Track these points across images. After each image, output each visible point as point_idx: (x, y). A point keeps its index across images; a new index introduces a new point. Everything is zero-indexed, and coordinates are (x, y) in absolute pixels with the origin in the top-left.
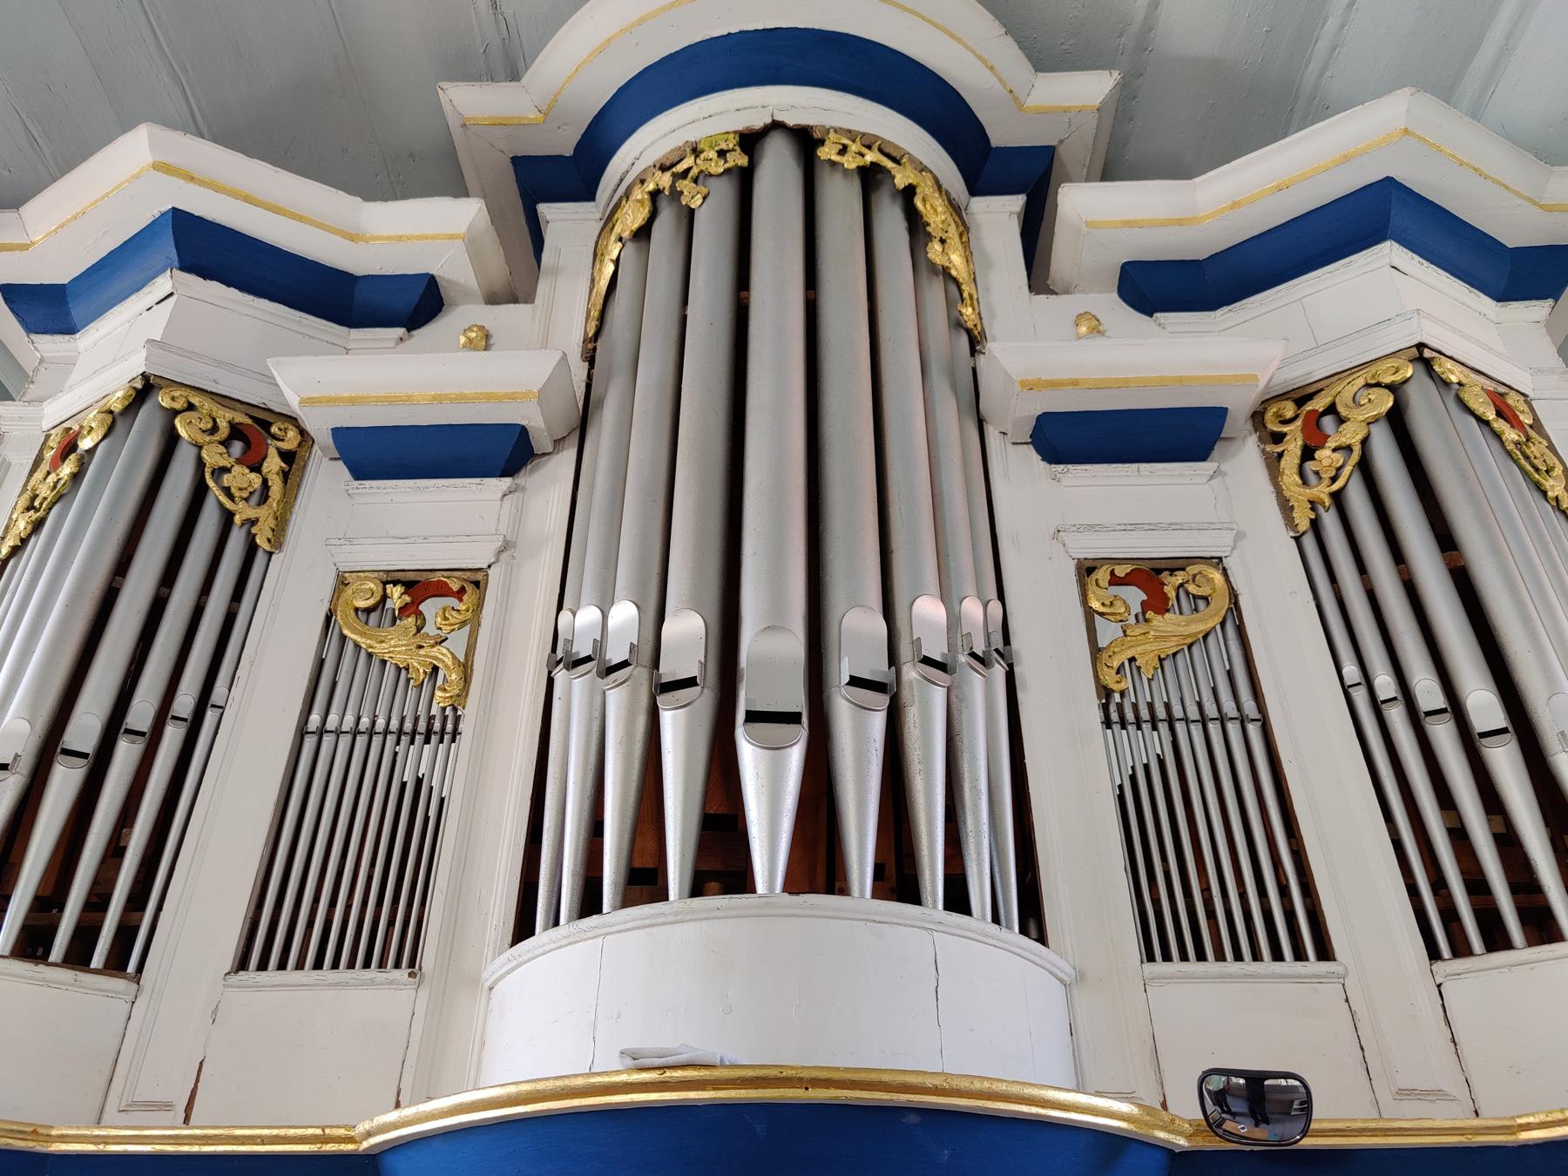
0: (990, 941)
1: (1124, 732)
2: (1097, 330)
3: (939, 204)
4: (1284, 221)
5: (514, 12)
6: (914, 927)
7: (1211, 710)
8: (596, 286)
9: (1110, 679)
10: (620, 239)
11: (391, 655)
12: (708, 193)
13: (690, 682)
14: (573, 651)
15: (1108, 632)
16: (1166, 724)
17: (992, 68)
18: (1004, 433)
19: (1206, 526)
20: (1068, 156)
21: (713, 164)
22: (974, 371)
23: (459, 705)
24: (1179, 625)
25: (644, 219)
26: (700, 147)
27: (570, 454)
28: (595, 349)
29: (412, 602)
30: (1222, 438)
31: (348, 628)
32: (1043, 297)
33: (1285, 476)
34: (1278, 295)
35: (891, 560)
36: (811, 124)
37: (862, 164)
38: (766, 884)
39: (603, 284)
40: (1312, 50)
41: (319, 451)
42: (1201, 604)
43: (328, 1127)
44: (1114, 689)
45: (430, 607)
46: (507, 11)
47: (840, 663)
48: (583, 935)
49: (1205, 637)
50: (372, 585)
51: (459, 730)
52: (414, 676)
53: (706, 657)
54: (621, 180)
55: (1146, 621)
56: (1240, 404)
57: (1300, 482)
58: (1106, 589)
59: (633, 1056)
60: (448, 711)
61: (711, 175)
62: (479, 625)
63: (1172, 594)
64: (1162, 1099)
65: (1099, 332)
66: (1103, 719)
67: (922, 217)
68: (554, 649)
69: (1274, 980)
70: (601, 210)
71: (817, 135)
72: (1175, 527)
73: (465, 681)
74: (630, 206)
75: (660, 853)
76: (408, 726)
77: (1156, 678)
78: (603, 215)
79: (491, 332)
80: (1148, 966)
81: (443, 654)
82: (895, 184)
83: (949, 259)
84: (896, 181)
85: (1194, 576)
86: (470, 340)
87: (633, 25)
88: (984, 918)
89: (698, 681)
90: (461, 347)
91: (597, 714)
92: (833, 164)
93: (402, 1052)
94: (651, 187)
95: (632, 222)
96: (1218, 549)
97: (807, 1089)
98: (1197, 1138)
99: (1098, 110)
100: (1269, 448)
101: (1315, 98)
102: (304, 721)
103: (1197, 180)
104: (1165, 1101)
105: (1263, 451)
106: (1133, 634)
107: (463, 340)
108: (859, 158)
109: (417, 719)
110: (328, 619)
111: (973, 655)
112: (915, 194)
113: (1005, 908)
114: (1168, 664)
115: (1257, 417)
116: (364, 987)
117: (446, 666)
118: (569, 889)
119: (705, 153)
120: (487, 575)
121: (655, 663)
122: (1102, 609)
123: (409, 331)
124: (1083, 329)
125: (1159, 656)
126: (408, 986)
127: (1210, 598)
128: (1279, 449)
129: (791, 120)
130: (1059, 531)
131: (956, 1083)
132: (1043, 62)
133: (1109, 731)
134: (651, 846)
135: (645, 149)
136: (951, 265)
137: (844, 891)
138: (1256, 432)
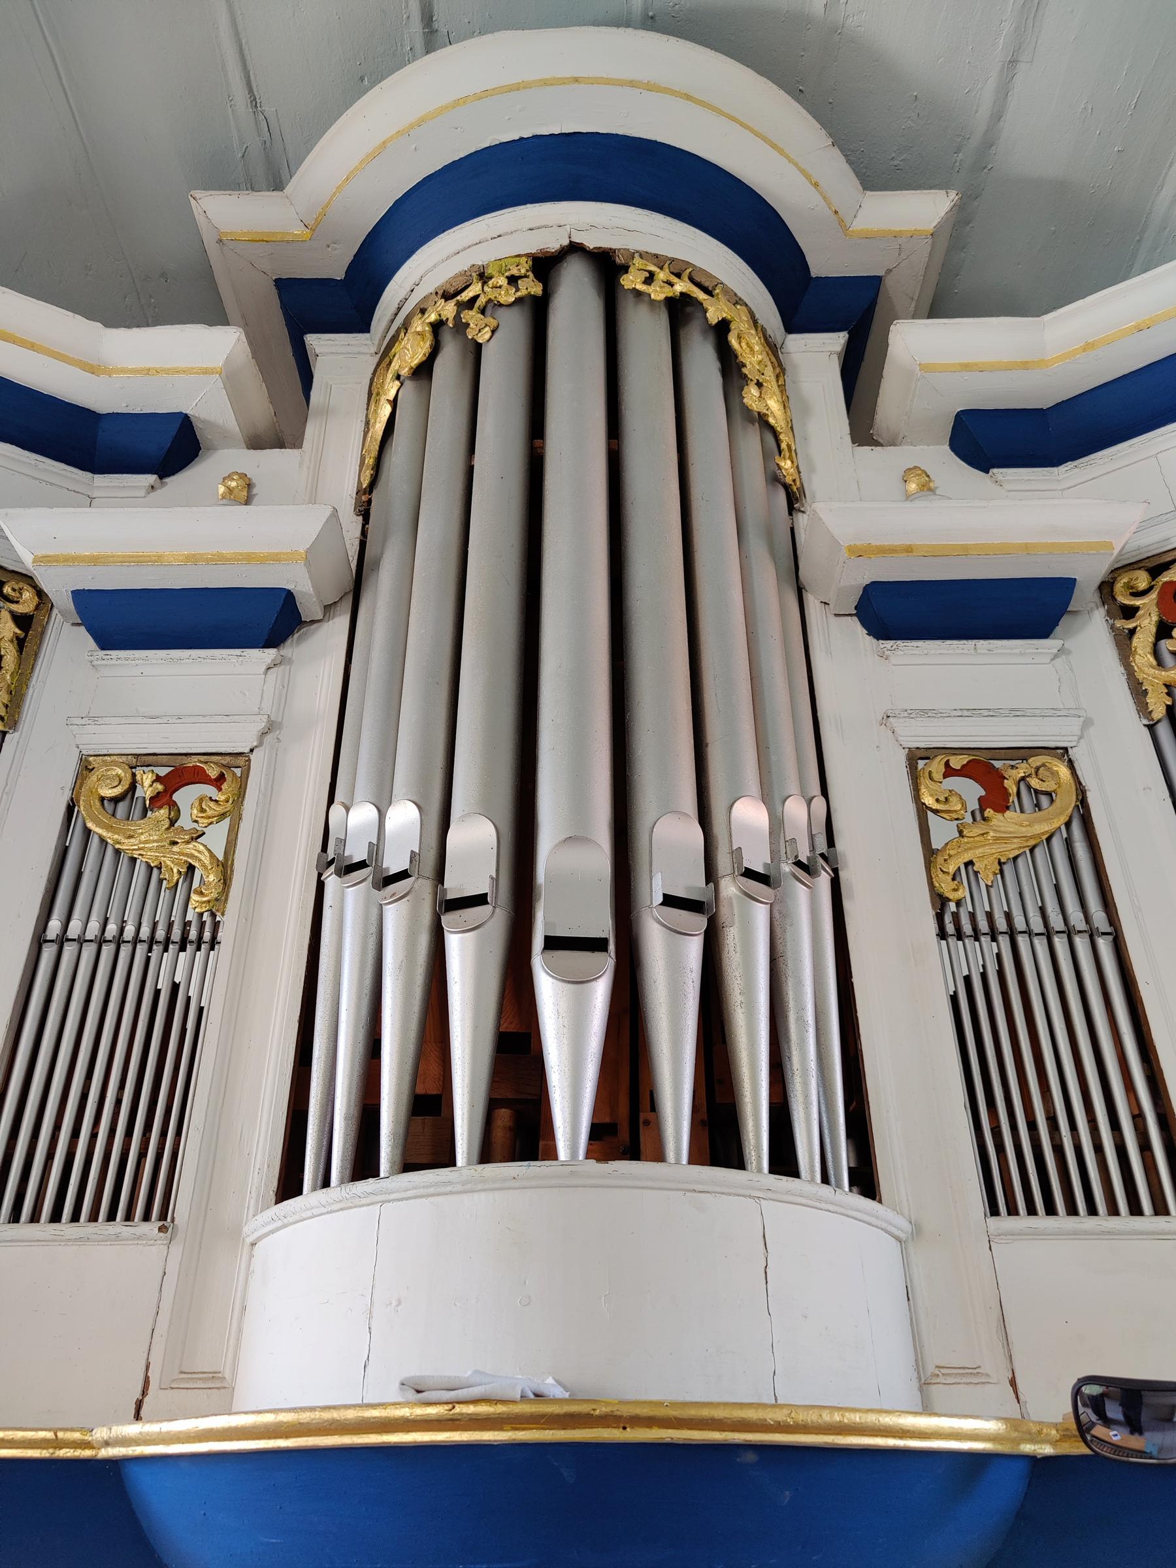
0: (823, 1205)
1: (960, 943)
2: (927, 488)
3: (756, 342)
4: (1141, 366)
6: (738, 1195)
7: (1056, 922)
8: (371, 430)
9: (945, 886)
10: (398, 377)
11: (142, 852)
12: (498, 327)
13: (481, 900)
14: (345, 855)
15: (942, 832)
16: (1007, 938)
17: (816, 185)
18: (825, 603)
19: (1051, 712)
20: (898, 289)
21: (503, 293)
22: (792, 530)
23: (217, 910)
25: (425, 355)
26: (489, 271)
27: (342, 622)
28: (369, 502)
29: (165, 791)
30: (1069, 611)
31: (92, 820)
32: (867, 448)
33: (1137, 656)
34: (1131, 450)
35: (706, 755)
36: (613, 247)
37: (670, 295)
38: (568, 1143)
39: (379, 427)
40: (1166, 174)
41: (59, 615)
42: (1044, 800)
43: (61, 1430)
44: (951, 897)
45: (186, 796)
46: (269, 109)
47: (651, 879)
48: (357, 1201)
49: (1049, 840)
50: (120, 771)
51: (218, 939)
52: (167, 877)
53: (497, 871)
54: (399, 309)
55: (984, 819)
57: (1154, 663)
58: (941, 782)
59: (416, 1387)
60: (206, 917)
61: (501, 305)
62: (240, 819)
63: (1013, 789)
64: (1010, 1376)
65: (930, 490)
66: (938, 931)
67: (736, 357)
68: (324, 848)
69: (1135, 1237)
70: (376, 342)
71: (620, 260)
72: (1017, 713)
73: (225, 883)
74: (408, 340)
75: (444, 1078)
76: (160, 934)
77: (995, 884)
78: (380, 345)
79: (254, 481)
80: (992, 1221)
81: (199, 852)
82: (706, 319)
83: (767, 405)
84: (707, 314)
85: (1037, 769)
86: (230, 490)
87: (411, 127)
88: (813, 1180)
89: (489, 899)
90: (220, 497)
91: (373, 929)
92: (638, 294)
93: (151, 1321)
94: (433, 317)
95: (412, 358)
96: (1065, 738)
97: (624, 1428)
98: (1063, 1444)
99: (932, 235)
100: (1119, 623)
101: (1165, 228)
102: (42, 927)
103: (1047, 318)
104: (1014, 1377)
105: (1112, 627)
106: (971, 834)
107: (222, 489)
108: (667, 288)
109: (170, 925)
110: (70, 809)
111: (799, 864)
112: (729, 330)
113: (832, 1153)
114: (1008, 869)
115: (1106, 589)
116: (109, 1243)
117: (204, 865)
118: (342, 1135)
119: (493, 280)
120: (249, 760)
121: (440, 875)
122: (936, 806)
123: (161, 478)
124: (912, 487)
125: (999, 860)
126: (158, 1242)
127: (1054, 795)
128: (1131, 625)
129: (591, 242)
130: (888, 717)
131: (802, 1417)
133: (944, 942)
134: (435, 1069)
135: (426, 274)
136: (769, 413)
137: (659, 1156)
138: (1104, 605)
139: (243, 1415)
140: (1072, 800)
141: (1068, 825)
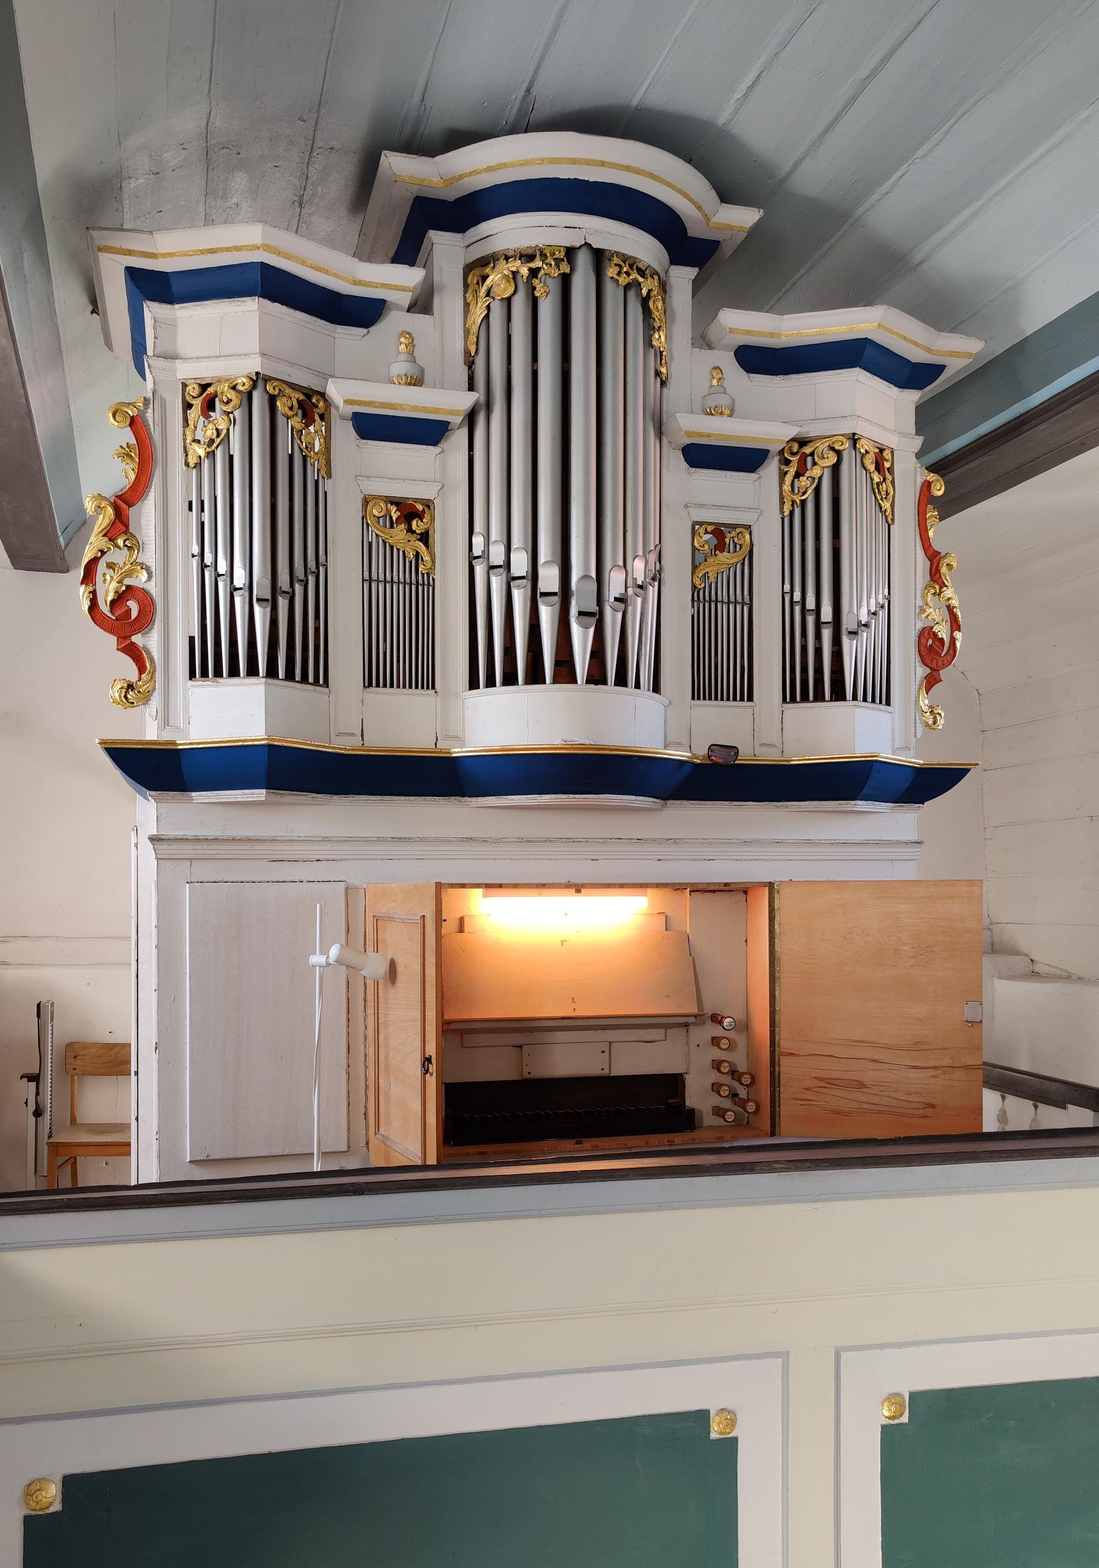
5: (432, 106)
9: (697, 582)
24: (728, 559)
27: (465, 431)
56: (775, 448)
82: (641, 293)
100: (783, 467)
105: (780, 468)
132: (726, 196)
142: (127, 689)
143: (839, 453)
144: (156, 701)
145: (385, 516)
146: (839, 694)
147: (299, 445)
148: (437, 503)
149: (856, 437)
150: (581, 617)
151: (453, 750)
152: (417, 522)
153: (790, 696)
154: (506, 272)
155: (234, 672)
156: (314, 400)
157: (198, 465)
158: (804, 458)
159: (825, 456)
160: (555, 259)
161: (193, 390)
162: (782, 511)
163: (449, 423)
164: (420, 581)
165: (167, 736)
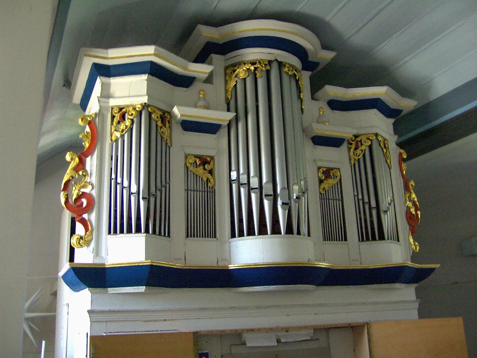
9: (321, 191)
27: (226, 130)
88: (306, 236)
100: (349, 146)
105: (348, 146)
132: (325, 47)
139: (125, 263)
140: (339, 178)
141: (337, 183)
142: (80, 239)
143: (371, 140)
144: (93, 244)
145: (194, 163)
146: (382, 237)
147: (161, 134)
148: (216, 158)
149: (377, 135)
150: (283, 205)
151: (229, 266)
152: (208, 165)
153: (362, 239)
154: (245, 69)
155: (129, 231)
156: (166, 115)
157: (117, 141)
158: (357, 142)
159: (366, 141)
160: (264, 64)
161: (116, 110)
162: (350, 163)
163: (222, 125)
164: (209, 191)
165: (98, 261)
